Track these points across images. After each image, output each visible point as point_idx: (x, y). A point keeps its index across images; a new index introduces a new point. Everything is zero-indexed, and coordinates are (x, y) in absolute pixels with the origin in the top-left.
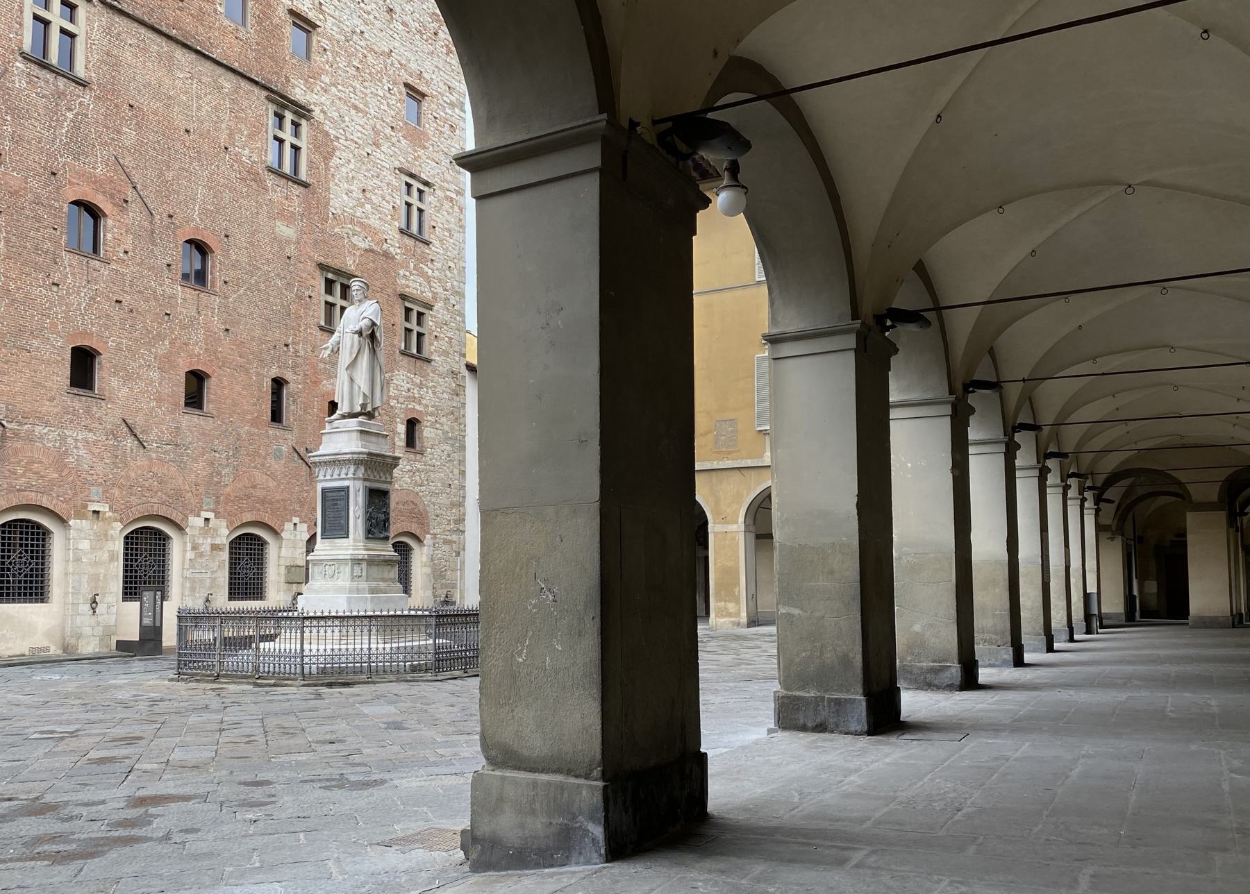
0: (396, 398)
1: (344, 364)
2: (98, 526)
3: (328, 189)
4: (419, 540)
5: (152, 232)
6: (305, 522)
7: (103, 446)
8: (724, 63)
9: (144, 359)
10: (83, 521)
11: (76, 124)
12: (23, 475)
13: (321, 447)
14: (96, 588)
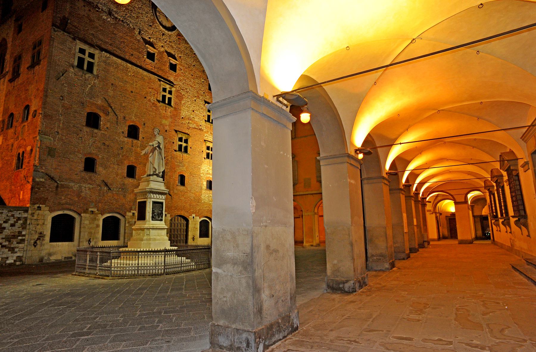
0: (203, 173)
2: (92, 216)
3: (181, 110)
4: (211, 219)
5: (117, 122)
6: (170, 214)
9: (112, 161)
10: (87, 214)
11: (91, 88)
12: (65, 199)
13: (139, 187)
14: (90, 236)
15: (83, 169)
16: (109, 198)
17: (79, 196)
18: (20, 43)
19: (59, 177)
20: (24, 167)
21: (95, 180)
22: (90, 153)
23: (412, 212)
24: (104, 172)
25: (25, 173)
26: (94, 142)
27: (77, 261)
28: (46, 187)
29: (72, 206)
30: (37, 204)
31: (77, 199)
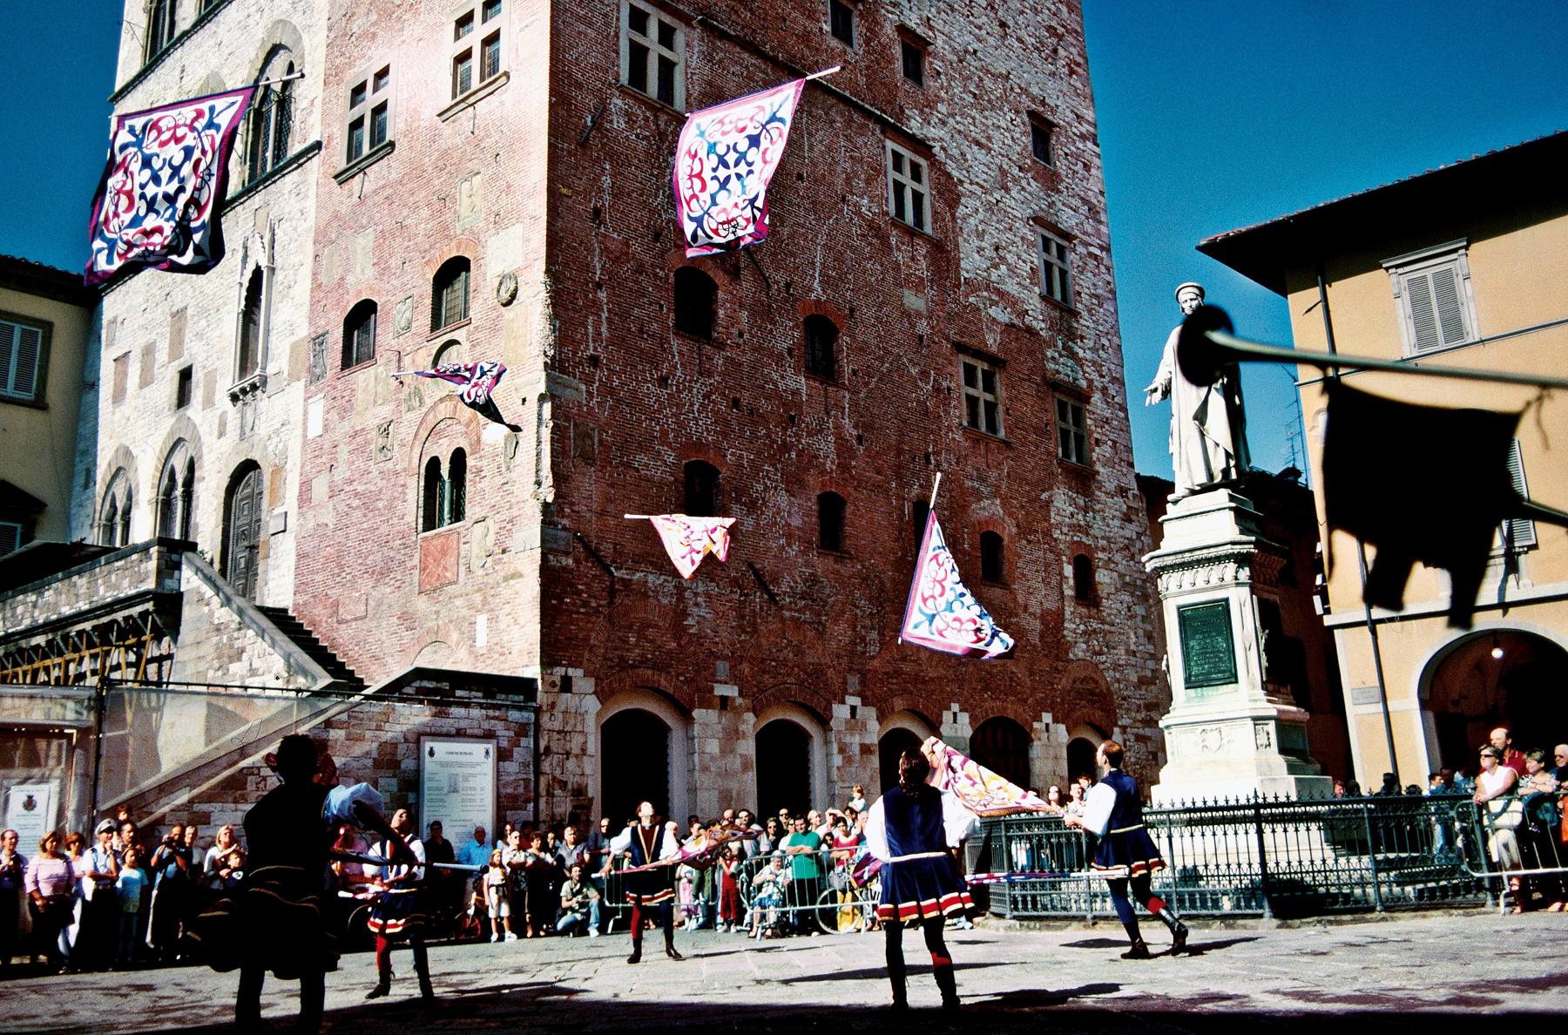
17: (678, 630)
18: (375, 24)
20: (471, 511)
22: (700, 446)
23: (1433, 319)
25: (491, 538)
26: (707, 396)
28: (579, 593)
29: (664, 675)
30: (561, 665)
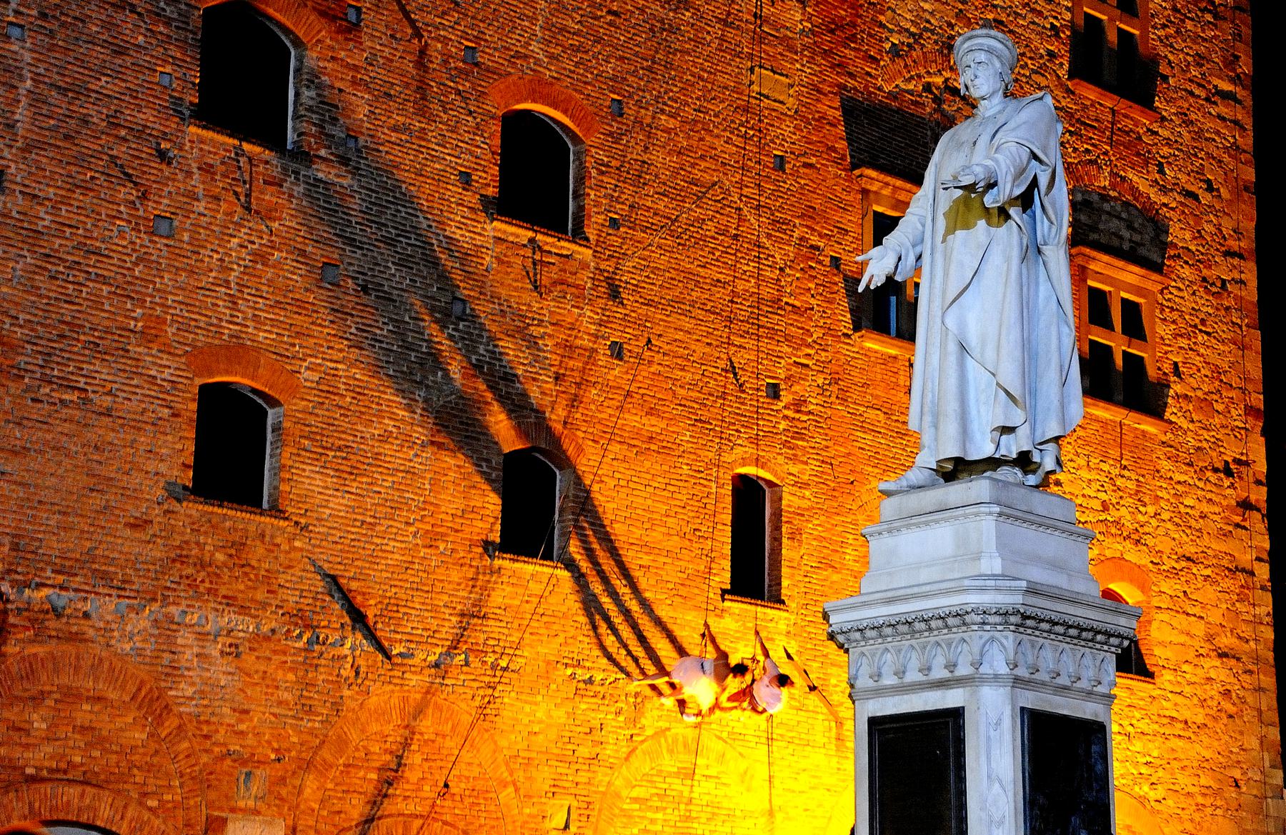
1: (944, 292)
7: (275, 652)
8: (913, 696)
15: (188, 478)
16: (375, 727)
19: (15, 547)
21: (269, 577)
24: (339, 503)
27: (1050, 48)
31: (140, 736)
